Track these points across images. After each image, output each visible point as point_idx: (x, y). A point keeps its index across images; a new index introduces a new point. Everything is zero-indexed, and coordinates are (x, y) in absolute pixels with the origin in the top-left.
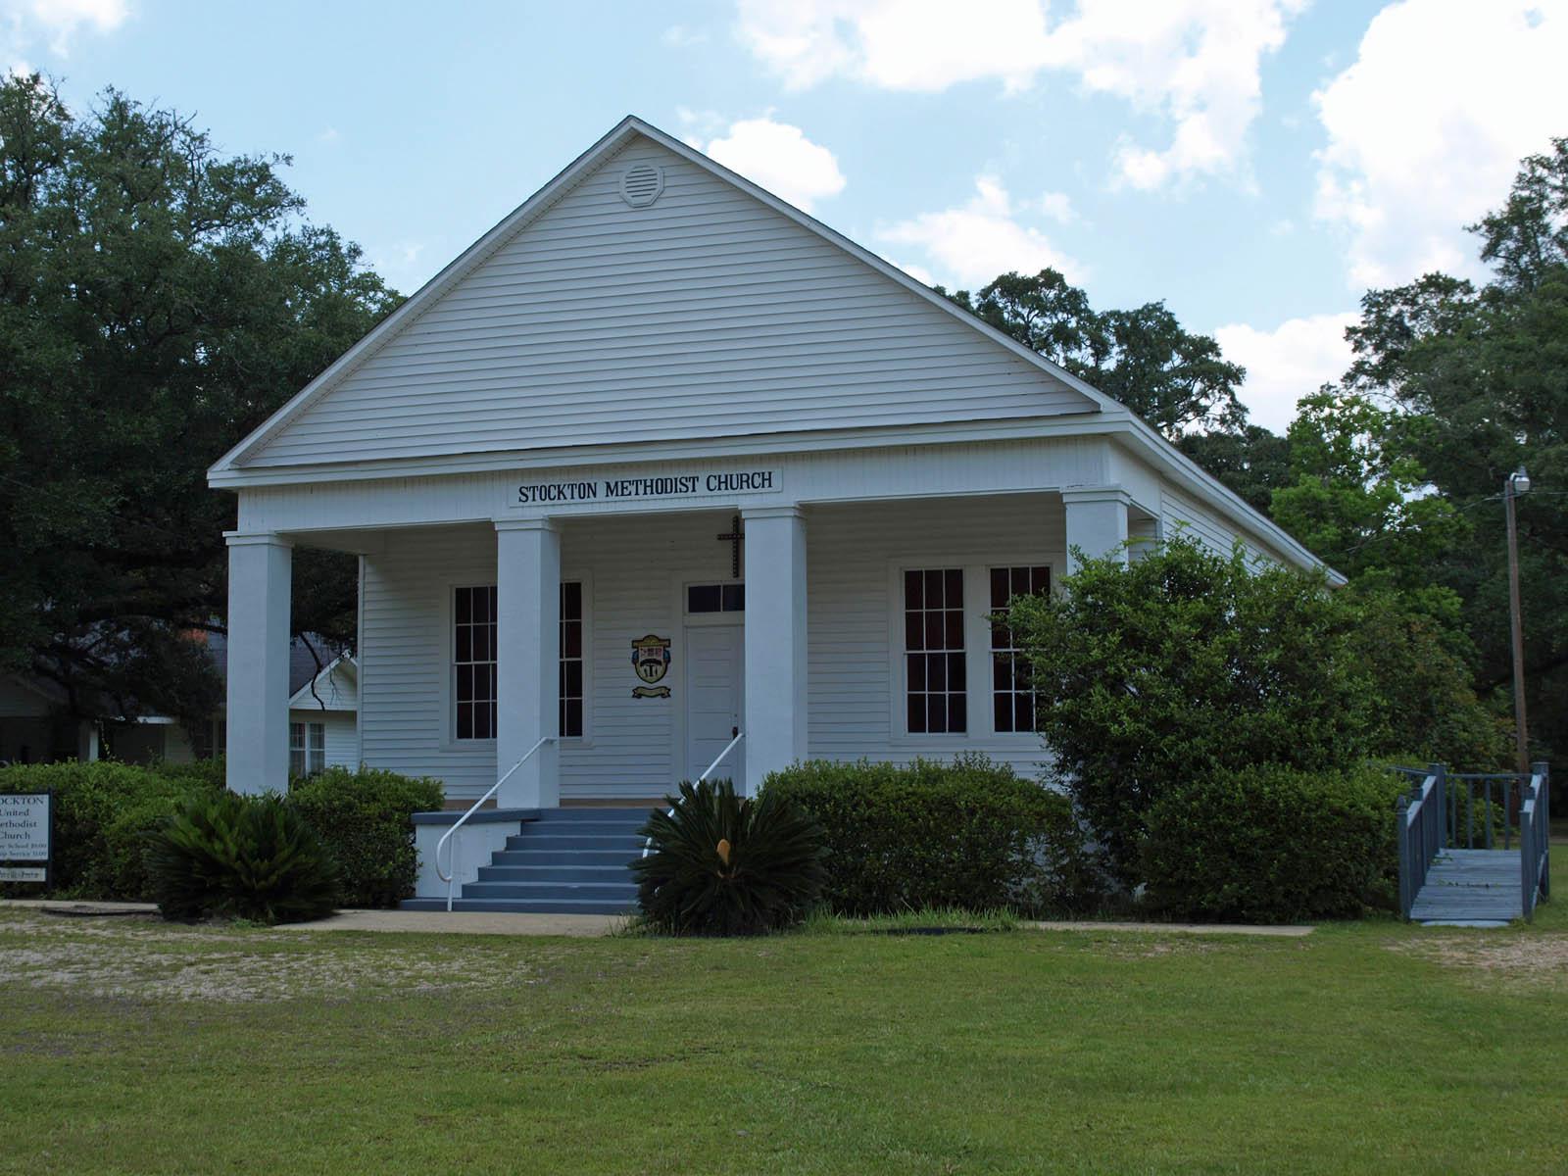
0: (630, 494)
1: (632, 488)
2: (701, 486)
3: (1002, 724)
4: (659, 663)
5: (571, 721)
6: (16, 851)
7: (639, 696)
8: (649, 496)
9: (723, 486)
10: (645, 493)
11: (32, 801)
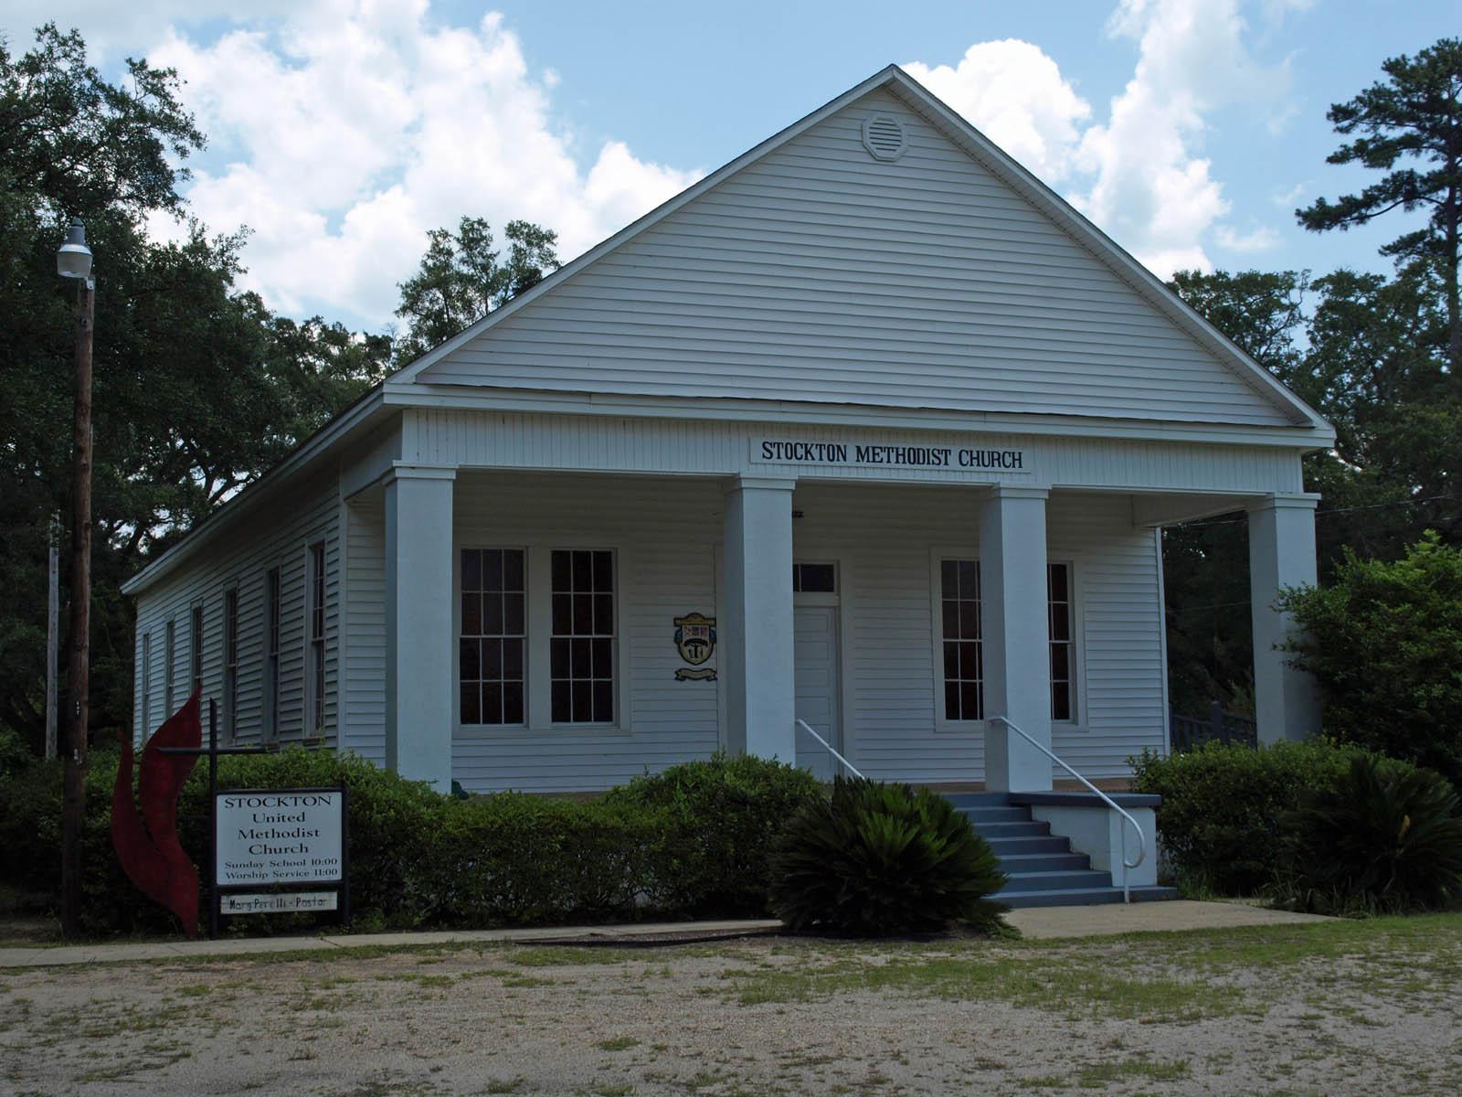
0: (881, 461)
1: (884, 455)
2: (953, 459)
3: (560, 714)
4: (704, 643)
5: (1061, 708)
6: (285, 869)
7: (684, 678)
8: (901, 465)
9: (975, 462)
10: (897, 462)
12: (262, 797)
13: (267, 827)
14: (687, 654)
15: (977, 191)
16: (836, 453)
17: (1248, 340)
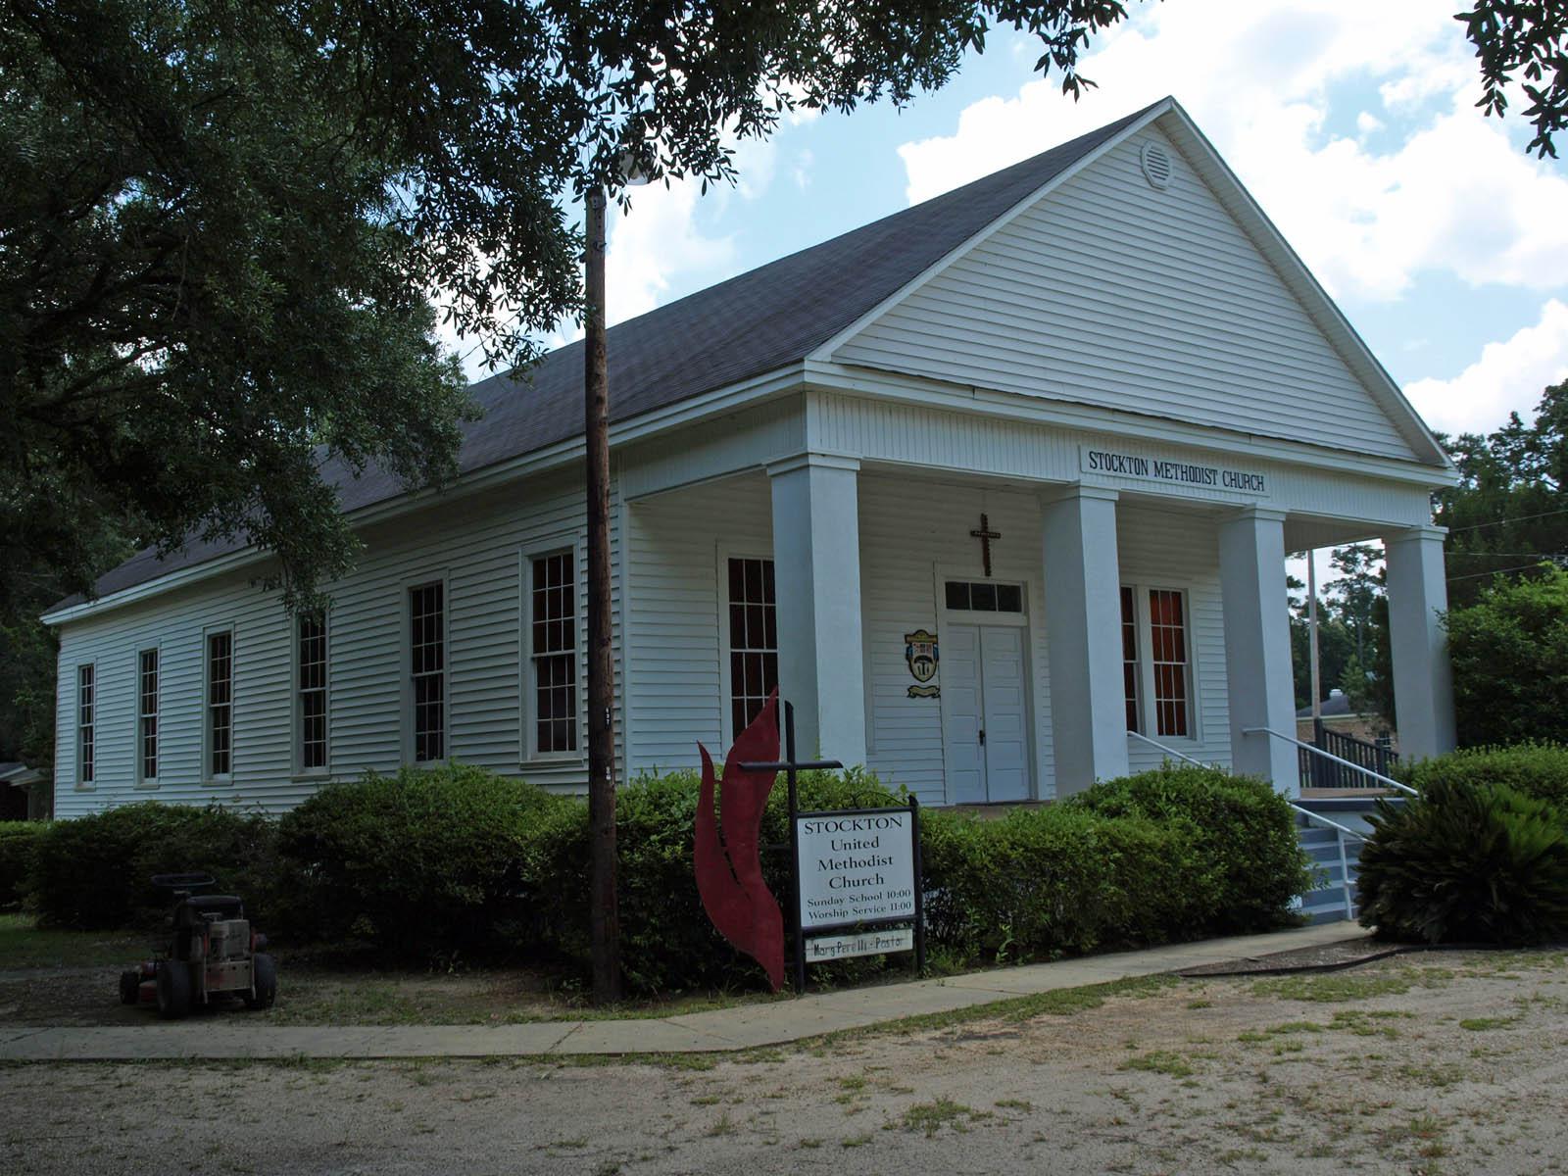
1: (1173, 471)
2: (1219, 478)
4: (930, 660)
6: (864, 905)
11: (882, 823)
12: (838, 820)
13: (843, 856)
14: (917, 672)
15: (1218, 226)
16: (1140, 467)
17: (145, 478)
